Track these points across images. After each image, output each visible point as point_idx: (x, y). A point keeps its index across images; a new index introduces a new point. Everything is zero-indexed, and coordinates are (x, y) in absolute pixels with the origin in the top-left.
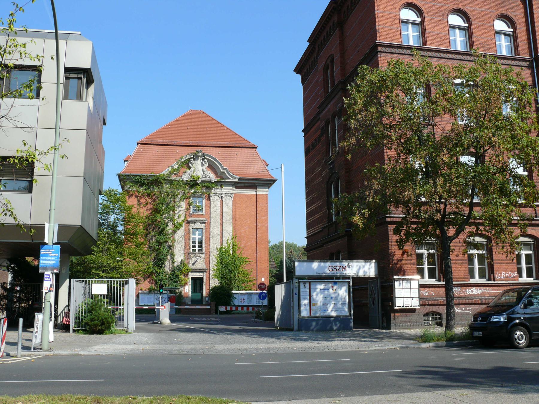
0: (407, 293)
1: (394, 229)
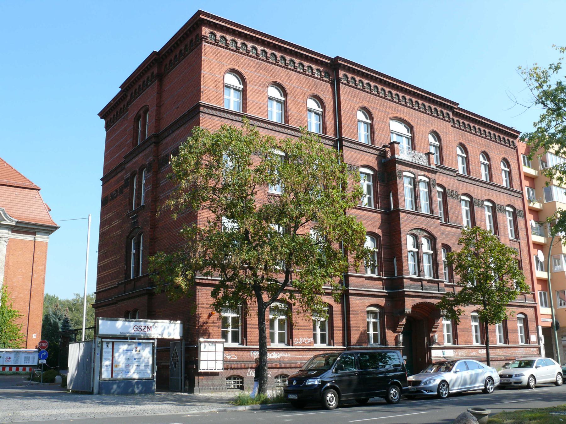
0: (212, 356)
1: (212, 292)
